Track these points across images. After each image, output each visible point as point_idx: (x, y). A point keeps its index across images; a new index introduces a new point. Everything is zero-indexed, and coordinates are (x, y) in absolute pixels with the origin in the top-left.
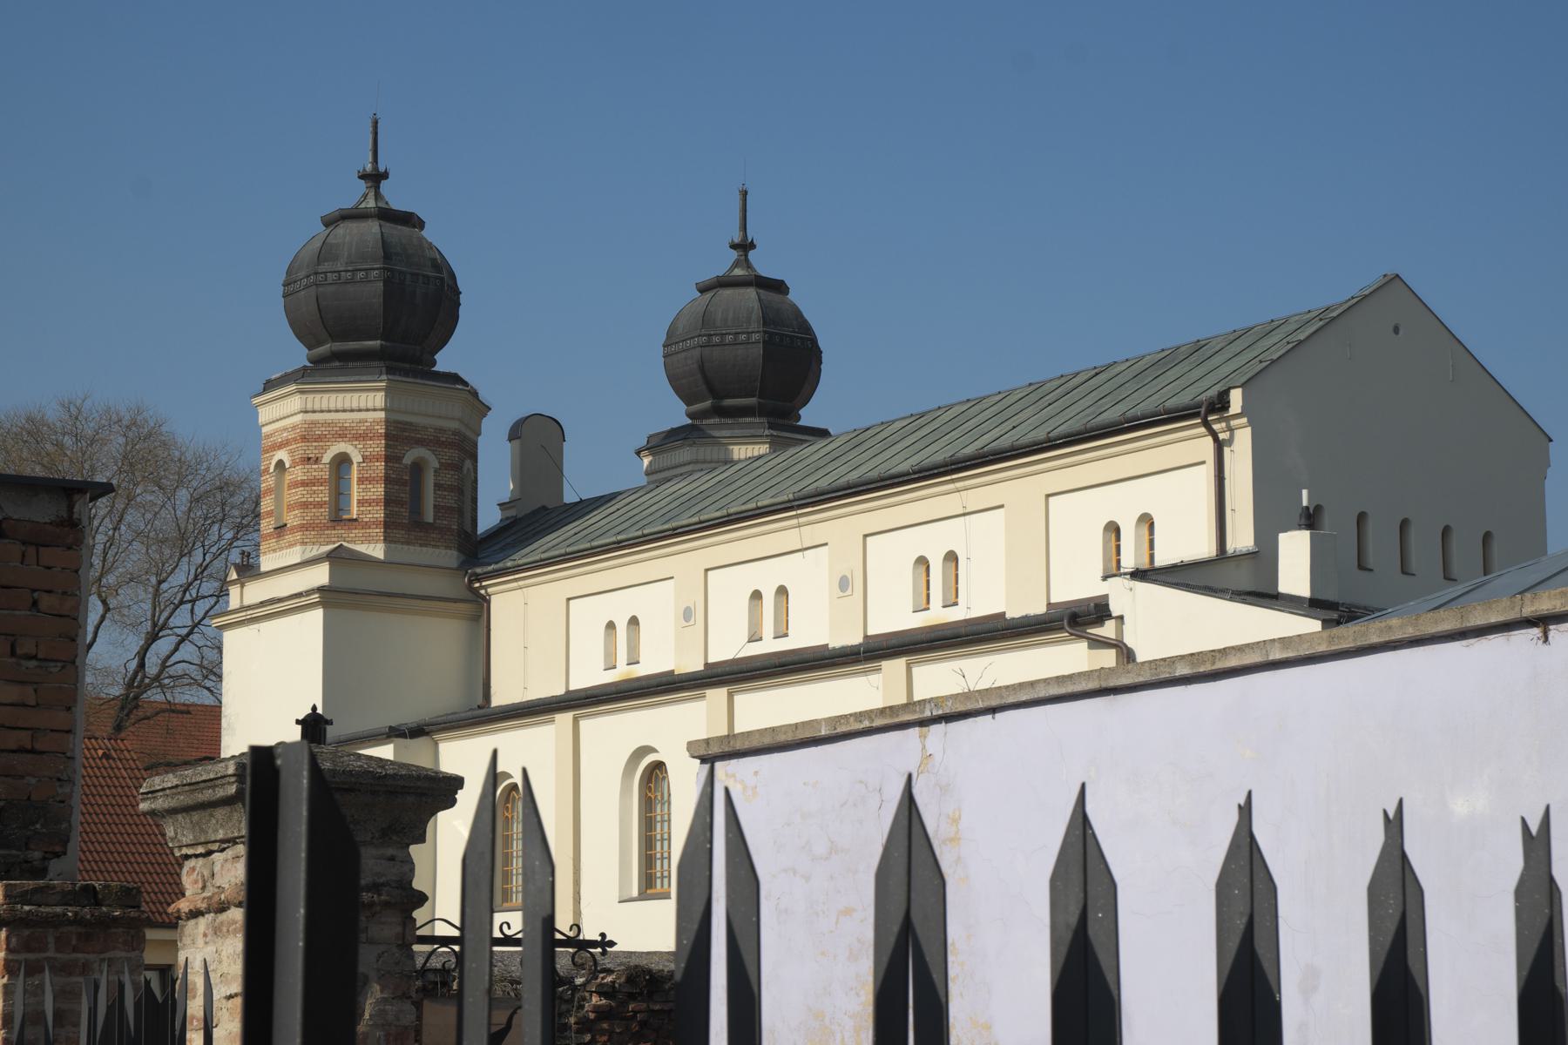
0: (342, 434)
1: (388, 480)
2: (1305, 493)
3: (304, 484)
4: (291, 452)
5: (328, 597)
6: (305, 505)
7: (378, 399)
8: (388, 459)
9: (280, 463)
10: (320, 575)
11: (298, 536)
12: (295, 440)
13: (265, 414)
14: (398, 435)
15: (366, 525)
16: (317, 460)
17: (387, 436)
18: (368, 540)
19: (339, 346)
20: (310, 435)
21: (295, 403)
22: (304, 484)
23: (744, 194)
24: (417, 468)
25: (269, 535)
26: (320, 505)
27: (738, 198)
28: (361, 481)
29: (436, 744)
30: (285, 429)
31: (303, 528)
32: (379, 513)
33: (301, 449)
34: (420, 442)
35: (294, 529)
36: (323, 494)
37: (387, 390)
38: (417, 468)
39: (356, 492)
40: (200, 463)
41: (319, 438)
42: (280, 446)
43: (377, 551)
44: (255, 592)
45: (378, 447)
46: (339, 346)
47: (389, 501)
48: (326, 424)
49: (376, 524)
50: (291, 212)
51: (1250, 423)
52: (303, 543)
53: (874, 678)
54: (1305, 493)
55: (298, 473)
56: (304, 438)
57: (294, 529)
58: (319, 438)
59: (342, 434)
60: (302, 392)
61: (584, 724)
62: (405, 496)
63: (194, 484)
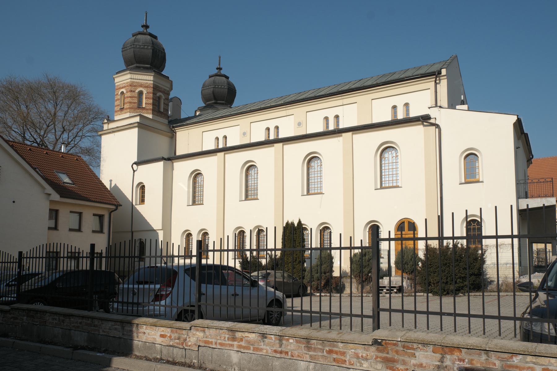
0: (141, 86)
1: (153, 99)
2: (462, 96)
3: (130, 97)
4: (126, 89)
5: (140, 125)
6: (130, 103)
7: (152, 78)
8: (153, 94)
9: (122, 93)
10: (137, 119)
11: (128, 110)
12: (128, 86)
13: (117, 80)
14: (156, 88)
15: (147, 110)
16: (134, 92)
17: (153, 88)
18: (148, 113)
19: (138, 65)
20: (132, 85)
21: (129, 76)
22: (130, 97)
23: (220, 57)
24: (159, 98)
25: (118, 111)
26: (135, 103)
27: (218, 59)
28: (146, 98)
29: (173, 163)
30: (124, 83)
31: (130, 108)
32: (151, 107)
33: (129, 88)
34: (160, 91)
35: (126, 109)
36: (136, 100)
37: (154, 76)
38: (159, 98)
39: (144, 101)
40: (91, 98)
41: (135, 86)
42: (122, 88)
43: (150, 116)
44: (112, 125)
45: (151, 90)
46: (138, 65)
47: (153, 104)
48: (137, 82)
49: (150, 109)
50: (125, 33)
51: (447, 78)
52: (130, 112)
53: (340, 139)
54: (462, 96)
55: (129, 94)
56: (130, 86)
57: (126, 109)
58: (135, 86)
59: (141, 86)
60: (131, 73)
61: (226, 155)
62: (157, 104)
63: (79, 109)
